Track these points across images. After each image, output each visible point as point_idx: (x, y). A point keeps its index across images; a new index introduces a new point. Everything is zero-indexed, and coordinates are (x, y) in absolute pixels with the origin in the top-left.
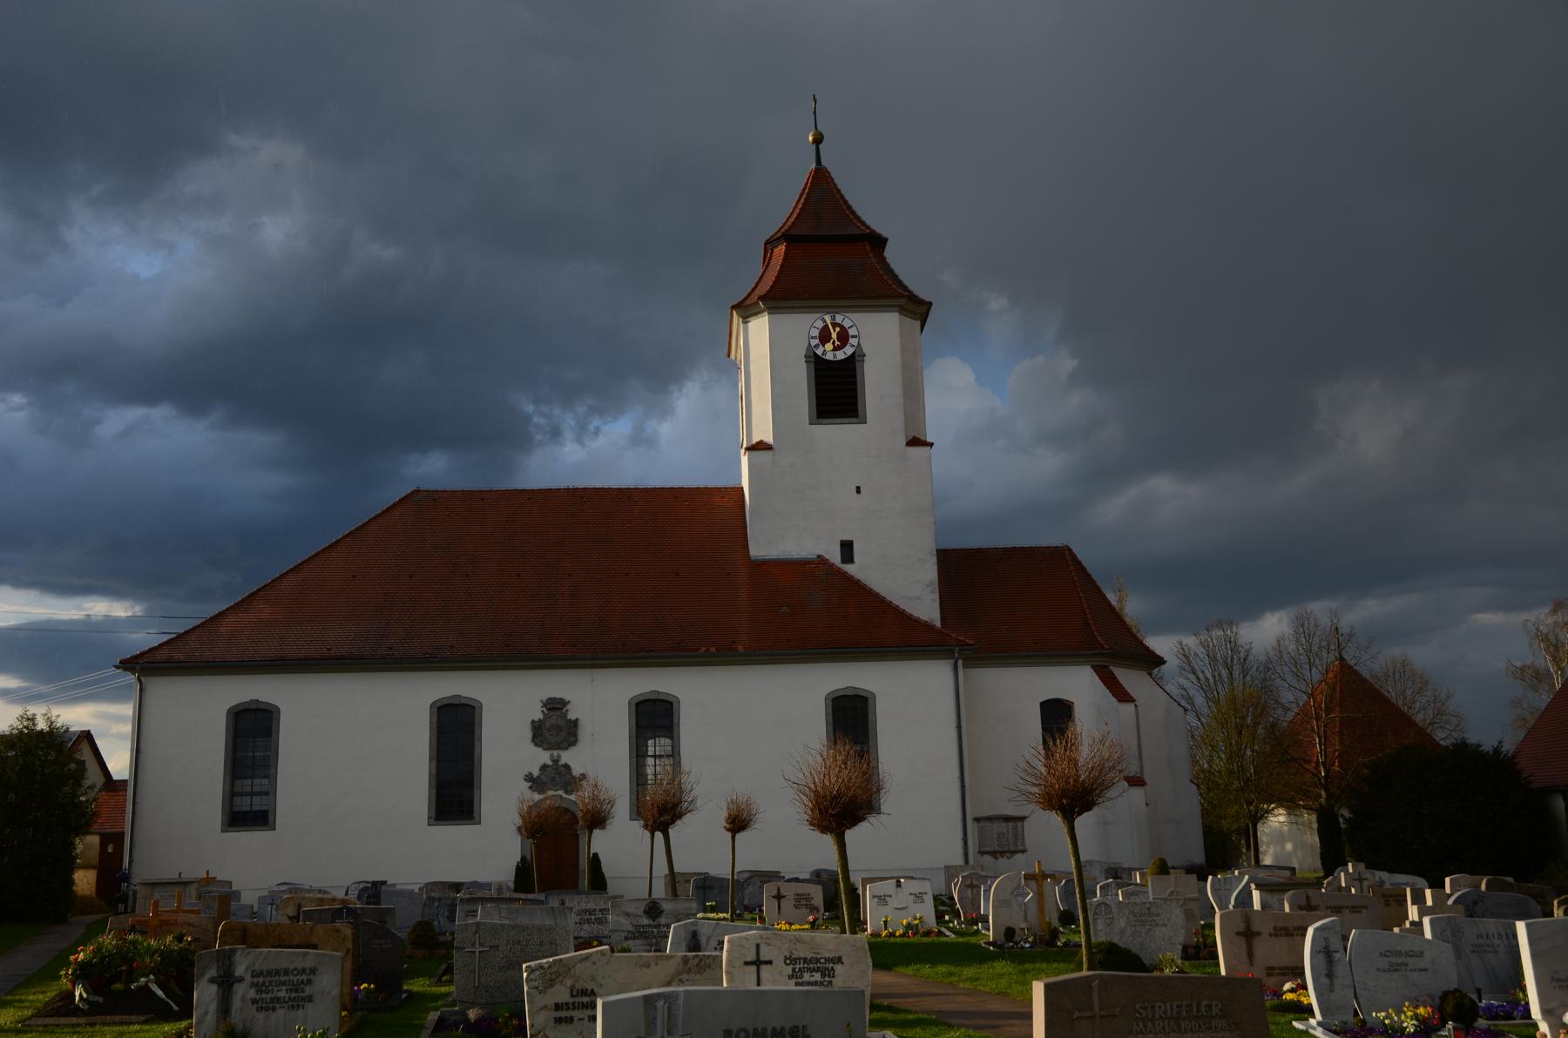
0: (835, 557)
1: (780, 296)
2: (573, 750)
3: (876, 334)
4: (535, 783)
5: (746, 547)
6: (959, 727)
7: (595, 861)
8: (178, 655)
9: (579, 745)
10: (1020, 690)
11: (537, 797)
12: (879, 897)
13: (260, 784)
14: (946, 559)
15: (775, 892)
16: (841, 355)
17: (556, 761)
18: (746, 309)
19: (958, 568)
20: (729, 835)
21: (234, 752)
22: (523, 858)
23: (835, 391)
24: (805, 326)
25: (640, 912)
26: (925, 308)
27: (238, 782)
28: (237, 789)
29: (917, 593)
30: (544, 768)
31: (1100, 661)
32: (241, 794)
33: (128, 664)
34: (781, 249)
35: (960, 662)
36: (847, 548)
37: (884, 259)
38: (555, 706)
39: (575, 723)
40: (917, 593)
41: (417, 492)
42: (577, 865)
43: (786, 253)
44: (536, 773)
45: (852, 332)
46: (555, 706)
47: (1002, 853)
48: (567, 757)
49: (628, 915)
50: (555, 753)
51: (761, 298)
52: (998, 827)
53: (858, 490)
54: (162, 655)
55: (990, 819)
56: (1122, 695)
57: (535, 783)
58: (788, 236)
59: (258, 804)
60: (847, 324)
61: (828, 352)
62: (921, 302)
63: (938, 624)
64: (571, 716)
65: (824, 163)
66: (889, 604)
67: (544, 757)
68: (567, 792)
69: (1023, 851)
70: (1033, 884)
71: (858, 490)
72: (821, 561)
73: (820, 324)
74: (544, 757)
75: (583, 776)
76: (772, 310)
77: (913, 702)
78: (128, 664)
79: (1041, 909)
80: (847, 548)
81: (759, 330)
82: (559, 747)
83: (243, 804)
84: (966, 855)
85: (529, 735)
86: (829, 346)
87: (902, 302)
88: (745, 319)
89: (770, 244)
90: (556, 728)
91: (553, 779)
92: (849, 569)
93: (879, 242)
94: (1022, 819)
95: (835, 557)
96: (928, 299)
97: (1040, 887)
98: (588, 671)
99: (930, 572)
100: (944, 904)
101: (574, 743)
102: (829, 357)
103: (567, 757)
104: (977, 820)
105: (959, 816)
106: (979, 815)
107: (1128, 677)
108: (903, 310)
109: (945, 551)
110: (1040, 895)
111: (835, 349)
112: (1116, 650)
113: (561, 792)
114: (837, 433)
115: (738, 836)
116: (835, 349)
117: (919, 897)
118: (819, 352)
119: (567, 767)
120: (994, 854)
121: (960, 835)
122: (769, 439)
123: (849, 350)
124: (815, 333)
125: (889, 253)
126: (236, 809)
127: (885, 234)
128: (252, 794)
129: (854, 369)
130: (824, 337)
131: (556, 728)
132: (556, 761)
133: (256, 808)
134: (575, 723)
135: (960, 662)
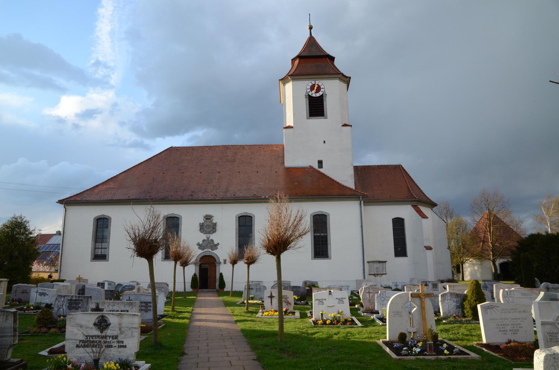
0: (316, 166)
1: (295, 75)
2: (214, 234)
3: (330, 88)
4: (200, 246)
5: (283, 163)
6: (362, 227)
7: (221, 275)
8: (78, 199)
9: (217, 232)
10: (383, 216)
11: (200, 251)
12: (319, 300)
13: (104, 245)
14: (357, 169)
15: (269, 295)
16: (318, 95)
17: (208, 238)
18: (284, 80)
19: (361, 172)
20: (246, 265)
21: (96, 233)
22: (195, 275)
23: (316, 107)
24: (305, 85)
25: (91, 324)
26: (348, 79)
27: (97, 244)
28: (97, 247)
29: (347, 180)
30: (204, 241)
31: (415, 203)
32: (98, 248)
33: (61, 202)
34: (297, 62)
35: (362, 202)
36: (320, 163)
37: (333, 65)
38: (208, 218)
39: (215, 224)
40: (347, 180)
41: (172, 147)
42: (215, 277)
43: (299, 62)
44: (201, 243)
45: (322, 87)
46: (208, 218)
47: (378, 274)
48: (212, 237)
49: (81, 326)
50: (208, 235)
51: (290, 76)
52: (376, 265)
53: (324, 142)
54: (72, 199)
55: (373, 262)
56: (424, 216)
57: (200, 246)
58: (299, 57)
59: (104, 252)
60: (320, 84)
61: (313, 94)
62: (347, 77)
63: (352, 186)
64: (214, 221)
65: (313, 35)
66: (335, 181)
67: (204, 236)
68: (212, 250)
69: (385, 274)
70: (417, 300)
71: (324, 142)
72: (311, 167)
73: (310, 84)
74: (204, 236)
75: (218, 244)
76: (293, 80)
77: (343, 216)
78: (61, 202)
79: (424, 318)
80: (320, 163)
81: (289, 86)
82: (209, 233)
83: (99, 252)
84: (364, 276)
85: (199, 228)
86: (313, 92)
87: (340, 76)
88: (284, 84)
89: (293, 60)
90: (208, 226)
91: (207, 245)
92: (321, 170)
93: (332, 59)
94: (385, 262)
95: (316, 166)
96: (349, 76)
97: (422, 303)
98: (221, 205)
99: (351, 172)
100: (355, 295)
101: (215, 232)
102: (314, 95)
103: (212, 237)
104: (368, 262)
105: (362, 261)
106: (369, 261)
107: (425, 210)
108: (341, 79)
109: (356, 167)
110: (422, 308)
111: (316, 93)
112: (419, 200)
113: (210, 250)
114: (317, 121)
115: (251, 266)
116: (316, 93)
117: (341, 300)
118: (310, 94)
119: (212, 240)
120: (374, 275)
121: (362, 268)
122: (292, 125)
123: (321, 93)
124: (309, 87)
125: (336, 63)
126: (96, 253)
127: (334, 56)
128: (101, 248)
129: (323, 100)
130: (312, 88)
131: (208, 226)
132: (208, 238)
133: (103, 253)
134: (215, 224)
135: (362, 202)
